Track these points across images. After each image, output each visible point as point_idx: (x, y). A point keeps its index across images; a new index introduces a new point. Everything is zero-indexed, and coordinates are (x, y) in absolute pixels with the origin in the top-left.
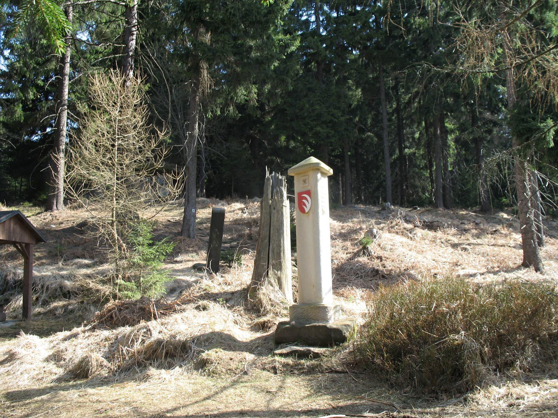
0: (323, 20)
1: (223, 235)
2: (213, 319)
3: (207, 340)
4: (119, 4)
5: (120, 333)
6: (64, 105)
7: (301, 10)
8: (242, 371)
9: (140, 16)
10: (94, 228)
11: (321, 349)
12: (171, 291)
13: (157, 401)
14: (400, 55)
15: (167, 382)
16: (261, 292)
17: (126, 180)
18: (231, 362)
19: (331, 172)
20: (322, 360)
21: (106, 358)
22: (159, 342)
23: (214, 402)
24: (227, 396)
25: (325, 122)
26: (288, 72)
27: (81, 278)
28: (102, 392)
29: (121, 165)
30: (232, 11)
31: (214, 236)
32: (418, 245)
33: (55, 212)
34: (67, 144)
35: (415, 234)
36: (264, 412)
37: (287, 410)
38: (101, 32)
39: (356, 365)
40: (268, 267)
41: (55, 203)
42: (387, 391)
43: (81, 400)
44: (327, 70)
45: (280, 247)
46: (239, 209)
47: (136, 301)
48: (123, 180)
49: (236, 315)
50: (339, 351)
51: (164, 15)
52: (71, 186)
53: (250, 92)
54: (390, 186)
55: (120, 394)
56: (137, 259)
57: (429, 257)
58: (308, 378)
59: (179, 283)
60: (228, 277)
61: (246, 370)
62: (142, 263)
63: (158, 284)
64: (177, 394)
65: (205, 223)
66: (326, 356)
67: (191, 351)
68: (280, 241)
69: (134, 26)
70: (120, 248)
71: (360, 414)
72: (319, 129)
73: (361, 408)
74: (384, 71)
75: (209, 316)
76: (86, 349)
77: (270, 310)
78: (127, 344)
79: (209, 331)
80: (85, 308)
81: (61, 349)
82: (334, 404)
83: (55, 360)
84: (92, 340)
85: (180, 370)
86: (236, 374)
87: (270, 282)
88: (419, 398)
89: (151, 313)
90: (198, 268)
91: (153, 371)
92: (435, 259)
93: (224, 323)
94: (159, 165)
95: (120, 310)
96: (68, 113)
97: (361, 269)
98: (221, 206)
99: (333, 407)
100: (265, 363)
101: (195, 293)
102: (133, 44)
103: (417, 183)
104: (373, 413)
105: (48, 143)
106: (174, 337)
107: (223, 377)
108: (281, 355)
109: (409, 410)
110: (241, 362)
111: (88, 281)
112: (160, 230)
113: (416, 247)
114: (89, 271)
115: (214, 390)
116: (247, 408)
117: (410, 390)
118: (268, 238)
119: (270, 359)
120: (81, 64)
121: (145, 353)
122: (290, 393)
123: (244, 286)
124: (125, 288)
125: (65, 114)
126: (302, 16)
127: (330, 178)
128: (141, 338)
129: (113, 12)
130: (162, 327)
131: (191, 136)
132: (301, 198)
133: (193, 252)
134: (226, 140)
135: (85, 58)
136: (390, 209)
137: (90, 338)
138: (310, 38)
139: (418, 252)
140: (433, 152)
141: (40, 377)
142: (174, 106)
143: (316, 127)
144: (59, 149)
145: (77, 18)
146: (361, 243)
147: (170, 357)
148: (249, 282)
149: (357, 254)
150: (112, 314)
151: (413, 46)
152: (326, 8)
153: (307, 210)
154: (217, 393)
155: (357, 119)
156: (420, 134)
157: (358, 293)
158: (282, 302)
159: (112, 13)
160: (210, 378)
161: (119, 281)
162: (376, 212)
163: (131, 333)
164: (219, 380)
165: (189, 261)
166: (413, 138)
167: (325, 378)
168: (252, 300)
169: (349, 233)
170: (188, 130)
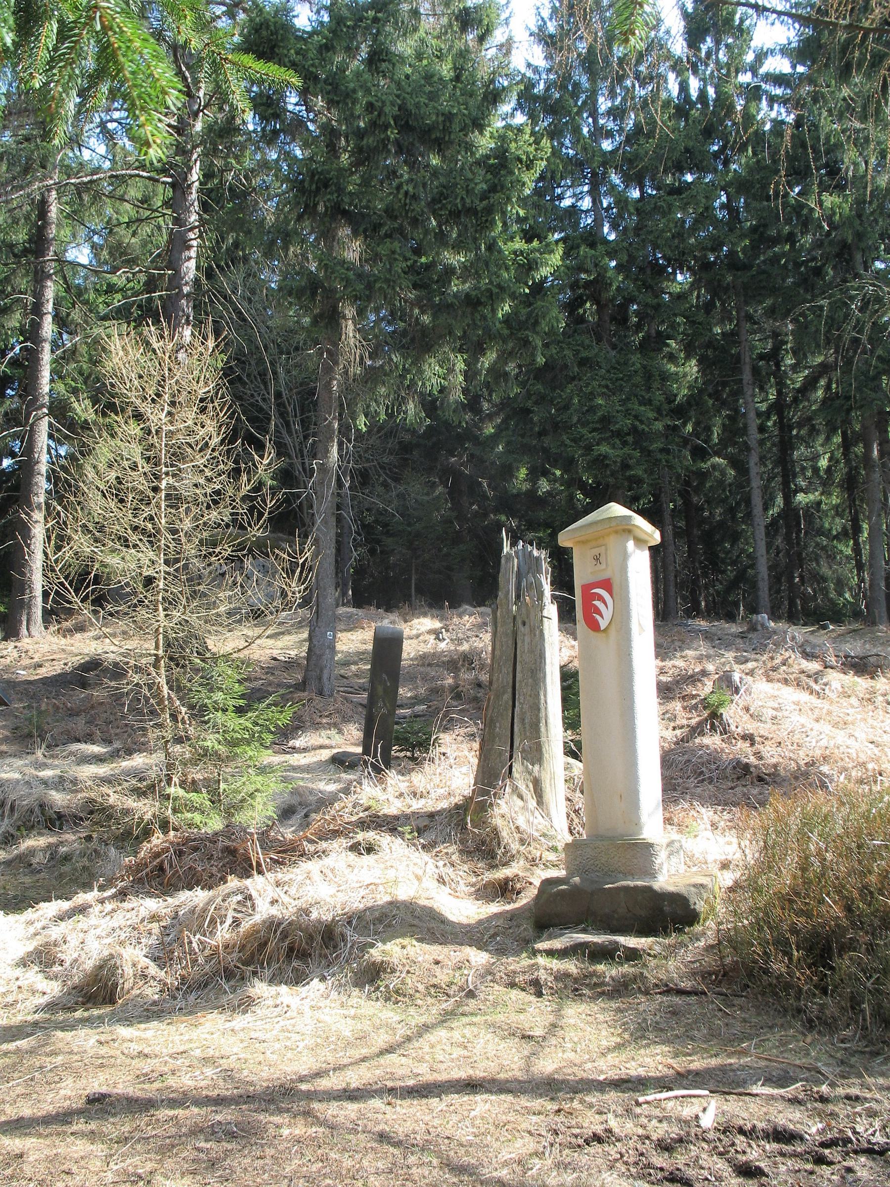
0: (609, 208)
1: (401, 691)
2: (391, 874)
3: (380, 920)
4: (157, 181)
5: (183, 903)
6: (43, 406)
7: (559, 186)
8: (462, 989)
9: (205, 207)
10: (117, 672)
11: (643, 940)
12: (286, 813)
13: (275, 1057)
14: (784, 280)
15: (295, 1014)
16: (497, 811)
17: (185, 566)
18: (437, 970)
19: (655, 536)
20: (645, 965)
21: (155, 960)
22: (272, 925)
23: (404, 1060)
24: (432, 1047)
25: (618, 434)
26: (536, 323)
27: (90, 783)
28: (149, 1034)
29: (174, 532)
30: (411, 189)
31: (380, 689)
32: (834, 708)
33: (25, 642)
34: (48, 492)
35: (826, 685)
36: (520, 1082)
37: (572, 1077)
38: (120, 244)
39: (723, 976)
40: (511, 757)
41: (25, 623)
42: (800, 1037)
43: (103, 1050)
44: (621, 318)
45: (539, 710)
46: (430, 632)
47: (216, 834)
48: (178, 565)
49: (441, 863)
50: (683, 945)
51: (257, 203)
52: (66, 578)
53: (451, 370)
54: (766, 577)
55: (190, 1041)
56: (211, 741)
57: (861, 736)
58: (614, 1005)
59: (300, 795)
60: (418, 779)
61: (471, 987)
62: (222, 749)
63: (259, 798)
64: (319, 1040)
65: (356, 663)
66: (655, 956)
67: (345, 945)
68: (538, 696)
69: (191, 229)
70: (174, 717)
71: (741, 1090)
72: (604, 449)
73: (742, 1075)
74: (749, 318)
75: (382, 866)
76: (109, 940)
77: (518, 852)
78: (200, 929)
79: (383, 899)
80: (95, 851)
81: (53, 938)
82: (679, 1063)
83: (41, 964)
84: (119, 919)
85: (322, 986)
86: (448, 995)
87: (515, 790)
88: (878, 1054)
89: (249, 859)
90: (341, 762)
91: (260, 988)
92: (875, 739)
93: (416, 882)
94: (256, 532)
95: (180, 854)
96: (50, 425)
97: (709, 762)
98: (389, 622)
99: (678, 1073)
100: (514, 972)
101: (346, 816)
102: (190, 268)
103: (825, 570)
104: (773, 1087)
105: (8, 489)
106: (307, 912)
107: (419, 1002)
108: (550, 953)
109: (857, 1081)
110: (460, 968)
111: (105, 789)
112: (256, 679)
113: (829, 713)
114: (103, 770)
115: (402, 1031)
116: (480, 1074)
117: (854, 1036)
118: (510, 690)
119: (525, 961)
120: (76, 315)
121: (242, 948)
122: (576, 1039)
123: (457, 799)
124: (186, 805)
125: (44, 426)
126: (561, 198)
127: (654, 551)
128: (231, 914)
129: (145, 200)
130: (278, 890)
131: (323, 468)
132: (589, 597)
133: (330, 726)
134: (397, 480)
135: (86, 302)
136: (767, 628)
137: (115, 915)
138: (583, 250)
139: (835, 725)
140: (862, 500)
141: (10, 999)
142: (280, 405)
143: (598, 444)
144: (29, 504)
145: (68, 216)
146: (705, 703)
147: (297, 957)
148: (468, 792)
149: (696, 730)
150: (162, 862)
151: (814, 259)
152: (615, 179)
153: (603, 624)
154: (409, 1039)
155: (689, 428)
156: (830, 459)
157: (705, 817)
158: (544, 835)
159: (142, 202)
160: (389, 1005)
161: (174, 790)
162: (736, 636)
163: (208, 904)
164: (412, 1010)
165: (321, 747)
166: (816, 470)
167: (653, 1006)
168: (476, 830)
169: (678, 682)
170: (314, 457)
